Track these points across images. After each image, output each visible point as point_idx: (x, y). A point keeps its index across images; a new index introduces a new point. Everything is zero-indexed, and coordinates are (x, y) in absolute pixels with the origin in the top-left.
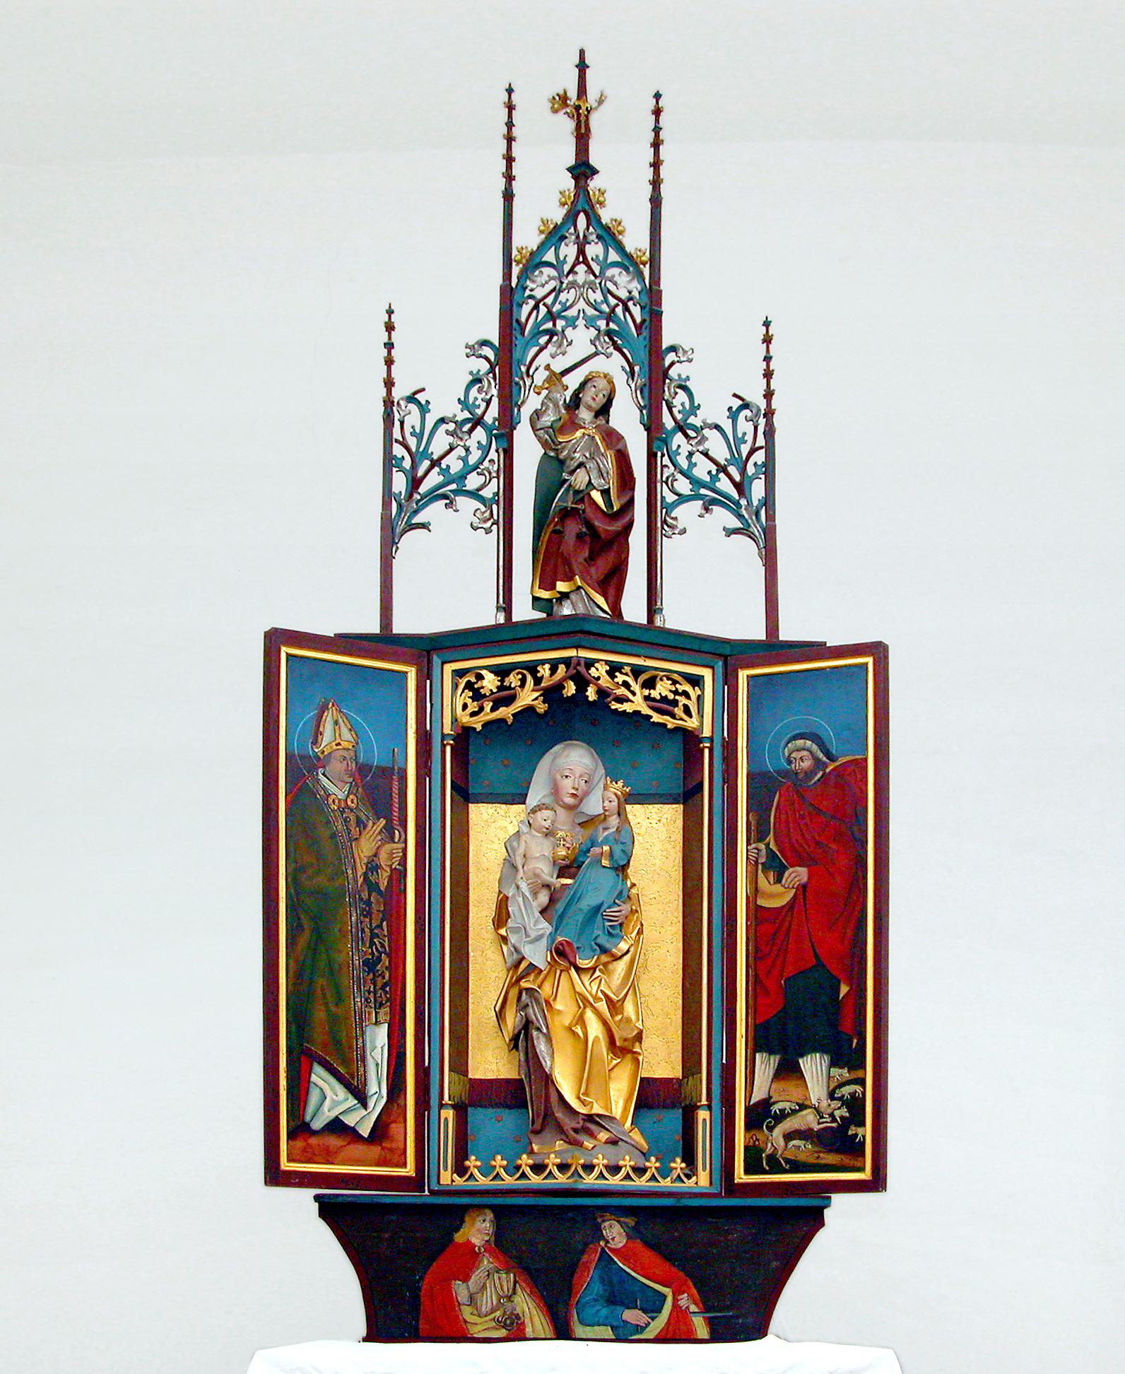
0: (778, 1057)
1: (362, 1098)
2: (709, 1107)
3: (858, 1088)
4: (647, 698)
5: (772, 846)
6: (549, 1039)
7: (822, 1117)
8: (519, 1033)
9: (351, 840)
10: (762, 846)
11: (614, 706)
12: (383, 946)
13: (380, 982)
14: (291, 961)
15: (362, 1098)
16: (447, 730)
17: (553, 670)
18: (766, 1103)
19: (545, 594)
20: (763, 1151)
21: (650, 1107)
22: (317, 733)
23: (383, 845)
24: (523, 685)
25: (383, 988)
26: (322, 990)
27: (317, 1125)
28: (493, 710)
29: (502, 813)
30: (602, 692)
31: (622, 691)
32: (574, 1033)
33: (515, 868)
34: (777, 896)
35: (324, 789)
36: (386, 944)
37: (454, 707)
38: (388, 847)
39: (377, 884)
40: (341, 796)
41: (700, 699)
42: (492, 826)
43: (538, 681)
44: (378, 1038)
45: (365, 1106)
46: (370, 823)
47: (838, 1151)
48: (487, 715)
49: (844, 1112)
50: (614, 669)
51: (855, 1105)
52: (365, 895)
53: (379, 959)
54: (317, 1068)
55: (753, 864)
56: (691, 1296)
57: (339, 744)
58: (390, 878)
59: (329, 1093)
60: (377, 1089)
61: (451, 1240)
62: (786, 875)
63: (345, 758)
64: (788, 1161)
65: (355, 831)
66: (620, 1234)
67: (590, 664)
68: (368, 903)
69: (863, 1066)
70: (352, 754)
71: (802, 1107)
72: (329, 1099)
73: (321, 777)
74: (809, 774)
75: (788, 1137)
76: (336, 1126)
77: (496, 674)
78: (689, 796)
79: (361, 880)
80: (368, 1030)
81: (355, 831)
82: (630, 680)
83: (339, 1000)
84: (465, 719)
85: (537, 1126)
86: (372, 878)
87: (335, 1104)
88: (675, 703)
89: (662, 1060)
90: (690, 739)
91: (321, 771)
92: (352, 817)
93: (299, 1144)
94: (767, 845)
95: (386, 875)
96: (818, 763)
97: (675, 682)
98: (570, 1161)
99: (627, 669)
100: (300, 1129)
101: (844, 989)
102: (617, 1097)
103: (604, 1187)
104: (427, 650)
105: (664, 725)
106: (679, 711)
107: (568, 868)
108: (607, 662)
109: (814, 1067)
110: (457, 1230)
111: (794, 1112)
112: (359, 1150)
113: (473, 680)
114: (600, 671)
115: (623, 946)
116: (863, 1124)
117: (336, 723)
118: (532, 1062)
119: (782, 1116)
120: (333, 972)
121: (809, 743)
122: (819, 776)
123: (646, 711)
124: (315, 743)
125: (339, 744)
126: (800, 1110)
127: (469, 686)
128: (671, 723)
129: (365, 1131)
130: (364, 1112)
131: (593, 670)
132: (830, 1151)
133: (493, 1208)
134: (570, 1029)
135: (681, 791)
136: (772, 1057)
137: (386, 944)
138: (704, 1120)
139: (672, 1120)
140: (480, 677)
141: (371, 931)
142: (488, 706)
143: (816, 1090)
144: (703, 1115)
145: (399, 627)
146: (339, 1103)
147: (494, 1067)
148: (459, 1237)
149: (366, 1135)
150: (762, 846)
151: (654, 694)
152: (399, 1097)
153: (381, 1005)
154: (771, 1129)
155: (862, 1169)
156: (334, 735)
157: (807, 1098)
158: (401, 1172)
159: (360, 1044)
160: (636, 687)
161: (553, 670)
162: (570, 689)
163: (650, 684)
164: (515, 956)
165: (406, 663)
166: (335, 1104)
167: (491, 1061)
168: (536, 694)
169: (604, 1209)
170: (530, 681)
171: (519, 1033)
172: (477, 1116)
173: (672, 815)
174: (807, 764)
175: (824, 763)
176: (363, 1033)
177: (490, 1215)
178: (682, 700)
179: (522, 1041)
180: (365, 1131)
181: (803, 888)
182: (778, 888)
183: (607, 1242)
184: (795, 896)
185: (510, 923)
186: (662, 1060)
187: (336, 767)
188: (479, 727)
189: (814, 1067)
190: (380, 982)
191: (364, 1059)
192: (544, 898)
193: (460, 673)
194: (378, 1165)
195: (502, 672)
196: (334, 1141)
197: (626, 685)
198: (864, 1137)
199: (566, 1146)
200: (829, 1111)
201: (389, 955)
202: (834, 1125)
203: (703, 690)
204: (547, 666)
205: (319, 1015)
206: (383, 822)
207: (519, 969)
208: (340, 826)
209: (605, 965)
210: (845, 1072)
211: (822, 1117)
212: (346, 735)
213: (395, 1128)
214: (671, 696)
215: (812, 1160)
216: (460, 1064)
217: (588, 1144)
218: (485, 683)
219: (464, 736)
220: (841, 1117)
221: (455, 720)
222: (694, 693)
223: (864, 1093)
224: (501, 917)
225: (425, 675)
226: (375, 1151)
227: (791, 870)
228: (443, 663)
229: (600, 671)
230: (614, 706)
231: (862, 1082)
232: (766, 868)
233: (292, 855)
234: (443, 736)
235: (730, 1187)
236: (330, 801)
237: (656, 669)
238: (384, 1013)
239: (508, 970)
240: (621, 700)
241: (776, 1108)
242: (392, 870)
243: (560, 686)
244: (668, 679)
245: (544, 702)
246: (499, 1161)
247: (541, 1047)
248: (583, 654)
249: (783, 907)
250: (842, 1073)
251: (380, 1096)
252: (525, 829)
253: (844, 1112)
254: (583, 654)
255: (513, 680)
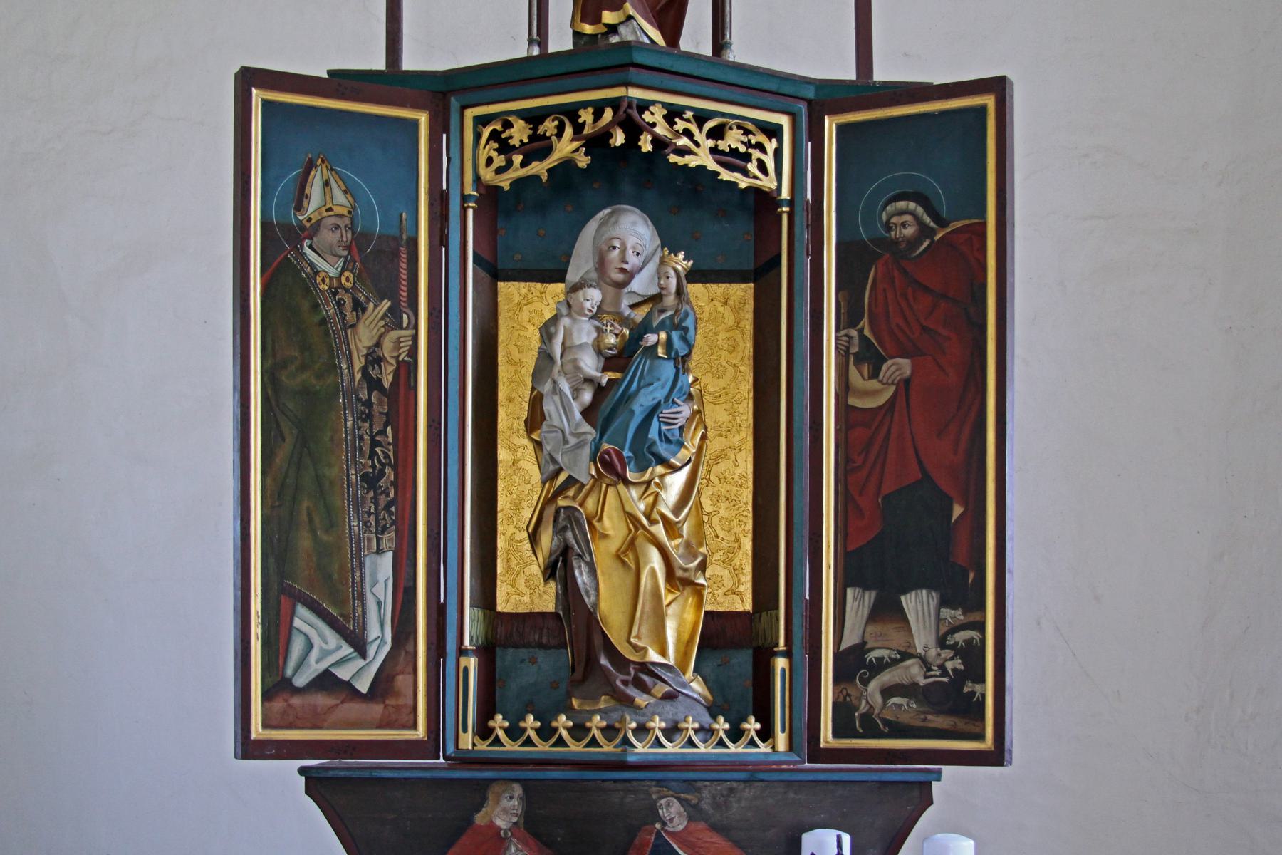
0: (874, 594)
1: (360, 647)
2: (788, 654)
3: (974, 634)
4: (714, 151)
5: (867, 332)
6: (593, 571)
7: (929, 669)
8: (556, 561)
9: (345, 327)
10: (854, 333)
11: (673, 158)
12: (386, 456)
13: (383, 500)
14: (269, 481)
15: (360, 647)
16: (470, 190)
17: (598, 115)
18: (860, 649)
19: (588, 29)
20: (857, 709)
21: (716, 648)
22: (300, 198)
23: (387, 332)
24: (560, 134)
25: (387, 507)
26: (309, 514)
27: (300, 681)
28: (524, 164)
29: (537, 293)
30: (658, 142)
31: (683, 141)
32: (624, 563)
33: (550, 358)
34: (874, 394)
35: (312, 265)
36: (391, 454)
37: (478, 163)
38: (394, 334)
39: (380, 380)
40: (333, 272)
41: (778, 153)
42: (526, 306)
43: (578, 128)
44: (382, 568)
45: (363, 655)
46: (371, 305)
47: (951, 712)
48: (516, 173)
49: (958, 664)
50: (673, 114)
51: (972, 655)
52: (364, 395)
53: (382, 473)
54: (301, 610)
55: (843, 355)
56: (766, 754)
57: (330, 210)
58: (396, 373)
59: (316, 641)
60: (379, 633)
61: (469, 821)
62: (884, 367)
63: (337, 227)
64: (887, 722)
65: (350, 316)
66: (680, 815)
67: (644, 106)
68: (368, 404)
69: (982, 606)
70: (347, 221)
71: (905, 656)
72: (316, 646)
73: (307, 250)
74: (913, 242)
75: (887, 692)
76: (326, 681)
77: (527, 120)
78: (762, 274)
79: (358, 376)
80: (368, 562)
81: (350, 316)
82: (693, 128)
83: (331, 525)
84: (488, 175)
85: (579, 674)
86: (373, 373)
87: (325, 654)
88: (747, 158)
89: (732, 591)
90: (763, 202)
91: (307, 242)
92: (348, 300)
93: (278, 705)
94: (861, 331)
95: (390, 369)
96: (924, 231)
97: (747, 132)
98: (617, 725)
99: (689, 114)
100: (277, 686)
101: (957, 511)
102: (680, 621)
103: (659, 758)
104: (446, 92)
105: (735, 184)
106: (752, 167)
107: (617, 360)
108: (664, 105)
109: (918, 606)
110: (478, 810)
111: (894, 662)
112: (354, 709)
113: (499, 127)
114: (655, 116)
115: (684, 454)
116: (982, 680)
117: (327, 183)
118: (569, 592)
119: (879, 667)
120: (322, 489)
121: (912, 205)
122: (926, 243)
123: (712, 165)
124: (299, 208)
125: (330, 210)
126: (902, 660)
127: (494, 136)
128: (743, 183)
129: (363, 686)
130: (361, 663)
131: (647, 117)
132: (938, 713)
133: (524, 783)
134: (619, 557)
135: (752, 267)
136: (867, 595)
137: (391, 454)
138: (783, 670)
139: (742, 660)
140: (508, 125)
141: (372, 437)
142: (518, 159)
143: (923, 639)
144: (781, 663)
145: (409, 63)
146: (329, 653)
147: (526, 598)
148: (480, 819)
149: (709, 54)
150: (854, 333)
151: (723, 145)
152: (407, 638)
153: (384, 529)
154: (865, 682)
155: (980, 737)
156: (324, 197)
157: (911, 644)
158: (407, 735)
159: (357, 578)
160: (699, 137)
161: (598, 115)
162: (619, 138)
163: (717, 133)
164: (552, 467)
165: (415, 106)
166: (325, 654)
167: (524, 588)
168: (576, 144)
169: (659, 783)
170: (569, 131)
171: (556, 561)
172: (506, 657)
173: (743, 292)
174: (909, 231)
175: (932, 229)
176: (361, 565)
177: (518, 790)
178: (756, 154)
179: (558, 568)
180: (363, 686)
181: (905, 385)
182: (874, 384)
183: (664, 824)
184: (894, 396)
185: (544, 428)
186: (732, 591)
187: (328, 237)
188: (506, 186)
189: (918, 606)
190: (383, 500)
191: (362, 597)
192: (587, 396)
193: (482, 121)
194: (380, 727)
195: (535, 118)
196: (322, 700)
197: (688, 133)
198: (983, 696)
199: (612, 703)
200: (939, 662)
201: (394, 467)
202: (945, 679)
203: (780, 142)
204: (590, 110)
205: (304, 542)
206: (386, 304)
207: (558, 485)
208: (331, 310)
209: (662, 476)
210: (959, 615)
211: (929, 669)
212: (340, 197)
213: (402, 681)
214: (742, 149)
215: (918, 723)
216: (486, 596)
217: (641, 699)
218: (512, 131)
219: (490, 198)
220: (955, 670)
221: (477, 179)
222: (771, 146)
223: (983, 641)
224: (535, 419)
225: (440, 125)
226: (376, 709)
227: (890, 362)
228: (464, 107)
229: (655, 116)
230: (673, 158)
231: (981, 627)
232: (859, 359)
233: (269, 347)
234: (465, 198)
235: (816, 754)
236: (319, 279)
237: (724, 115)
238: (389, 539)
239: (544, 483)
240: (682, 152)
241: (869, 646)
242: (398, 362)
243: (606, 134)
244: (739, 127)
245: (586, 154)
246: (530, 721)
247: (582, 577)
248: (635, 93)
249: (880, 408)
250: (954, 615)
251: (383, 642)
252: (564, 311)
253: (958, 664)
254: (635, 93)
255: (549, 126)
